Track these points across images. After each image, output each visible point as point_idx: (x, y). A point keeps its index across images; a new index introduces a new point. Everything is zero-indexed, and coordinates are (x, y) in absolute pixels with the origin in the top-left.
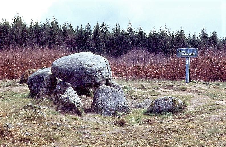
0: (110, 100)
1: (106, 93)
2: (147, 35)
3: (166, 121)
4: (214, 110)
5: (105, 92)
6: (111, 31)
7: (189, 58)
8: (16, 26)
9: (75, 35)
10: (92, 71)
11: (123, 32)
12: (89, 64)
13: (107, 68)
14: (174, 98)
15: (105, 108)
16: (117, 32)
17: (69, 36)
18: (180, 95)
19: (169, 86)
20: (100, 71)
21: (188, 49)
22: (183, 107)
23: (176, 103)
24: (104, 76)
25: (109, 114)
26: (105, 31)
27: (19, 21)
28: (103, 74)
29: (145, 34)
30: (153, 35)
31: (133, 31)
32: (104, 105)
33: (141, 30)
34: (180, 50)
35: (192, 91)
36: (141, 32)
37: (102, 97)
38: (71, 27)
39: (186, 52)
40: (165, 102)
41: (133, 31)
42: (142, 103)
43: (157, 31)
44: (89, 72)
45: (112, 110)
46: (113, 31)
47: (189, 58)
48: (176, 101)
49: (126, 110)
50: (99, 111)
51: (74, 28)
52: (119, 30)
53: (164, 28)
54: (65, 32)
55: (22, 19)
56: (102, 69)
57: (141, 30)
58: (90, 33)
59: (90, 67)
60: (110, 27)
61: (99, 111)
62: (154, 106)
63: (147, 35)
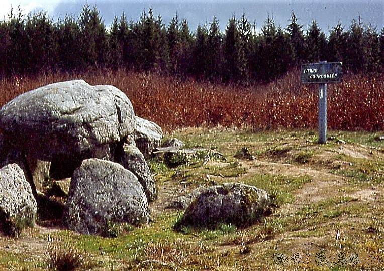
0: (103, 193)
1: (96, 178)
2: (328, 36)
3: (217, 241)
4: (333, 217)
5: (92, 175)
6: (257, 31)
7: (326, 85)
8: (86, 32)
9: (192, 42)
10: (68, 125)
11: (281, 32)
12: (65, 108)
13: (115, 117)
14: (247, 186)
15: (87, 213)
16: (269, 34)
17: (180, 45)
18: (287, 174)
19: (278, 151)
20: (87, 125)
21: (321, 65)
22: (266, 211)
23: (248, 200)
24: (98, 136)
25: (91, 229)
26: (246, 34)
27: (92, 20)
28: (96, 131)
29: (323, 35)
30: (337, 35)
31: (301, 30)
32: (86, 207)
33: (314, 27)
34: (308, 67)
35: (320, 162)
36: (315, 32)
37: (84, 186)
38: (185, 27)
39: (319, 73)
40: (221, 197)
41: (301, 30)
42: (185, 197)
43: (346, 29)
44: (62, 126)
45: (98, 218)
46: (262, 32)
47: (326, 85)
48: (249, 195)
49: (135, 218)
50: (70, 222)
51: (193, 31)
52: (273, 29)
53: (358, 22)
54: (173, 36)
55: (99, 16)
56: (93, 118)
57: (314, 27)
58: (219, 37)
59: (66, 116)
60: (256, 24)
61: (70, 222)
62: (195, 207)
63: (328, 36)
